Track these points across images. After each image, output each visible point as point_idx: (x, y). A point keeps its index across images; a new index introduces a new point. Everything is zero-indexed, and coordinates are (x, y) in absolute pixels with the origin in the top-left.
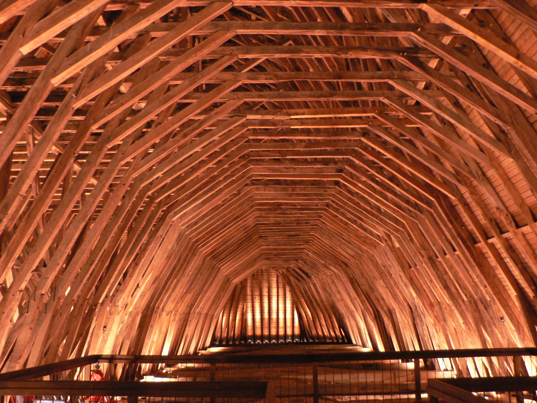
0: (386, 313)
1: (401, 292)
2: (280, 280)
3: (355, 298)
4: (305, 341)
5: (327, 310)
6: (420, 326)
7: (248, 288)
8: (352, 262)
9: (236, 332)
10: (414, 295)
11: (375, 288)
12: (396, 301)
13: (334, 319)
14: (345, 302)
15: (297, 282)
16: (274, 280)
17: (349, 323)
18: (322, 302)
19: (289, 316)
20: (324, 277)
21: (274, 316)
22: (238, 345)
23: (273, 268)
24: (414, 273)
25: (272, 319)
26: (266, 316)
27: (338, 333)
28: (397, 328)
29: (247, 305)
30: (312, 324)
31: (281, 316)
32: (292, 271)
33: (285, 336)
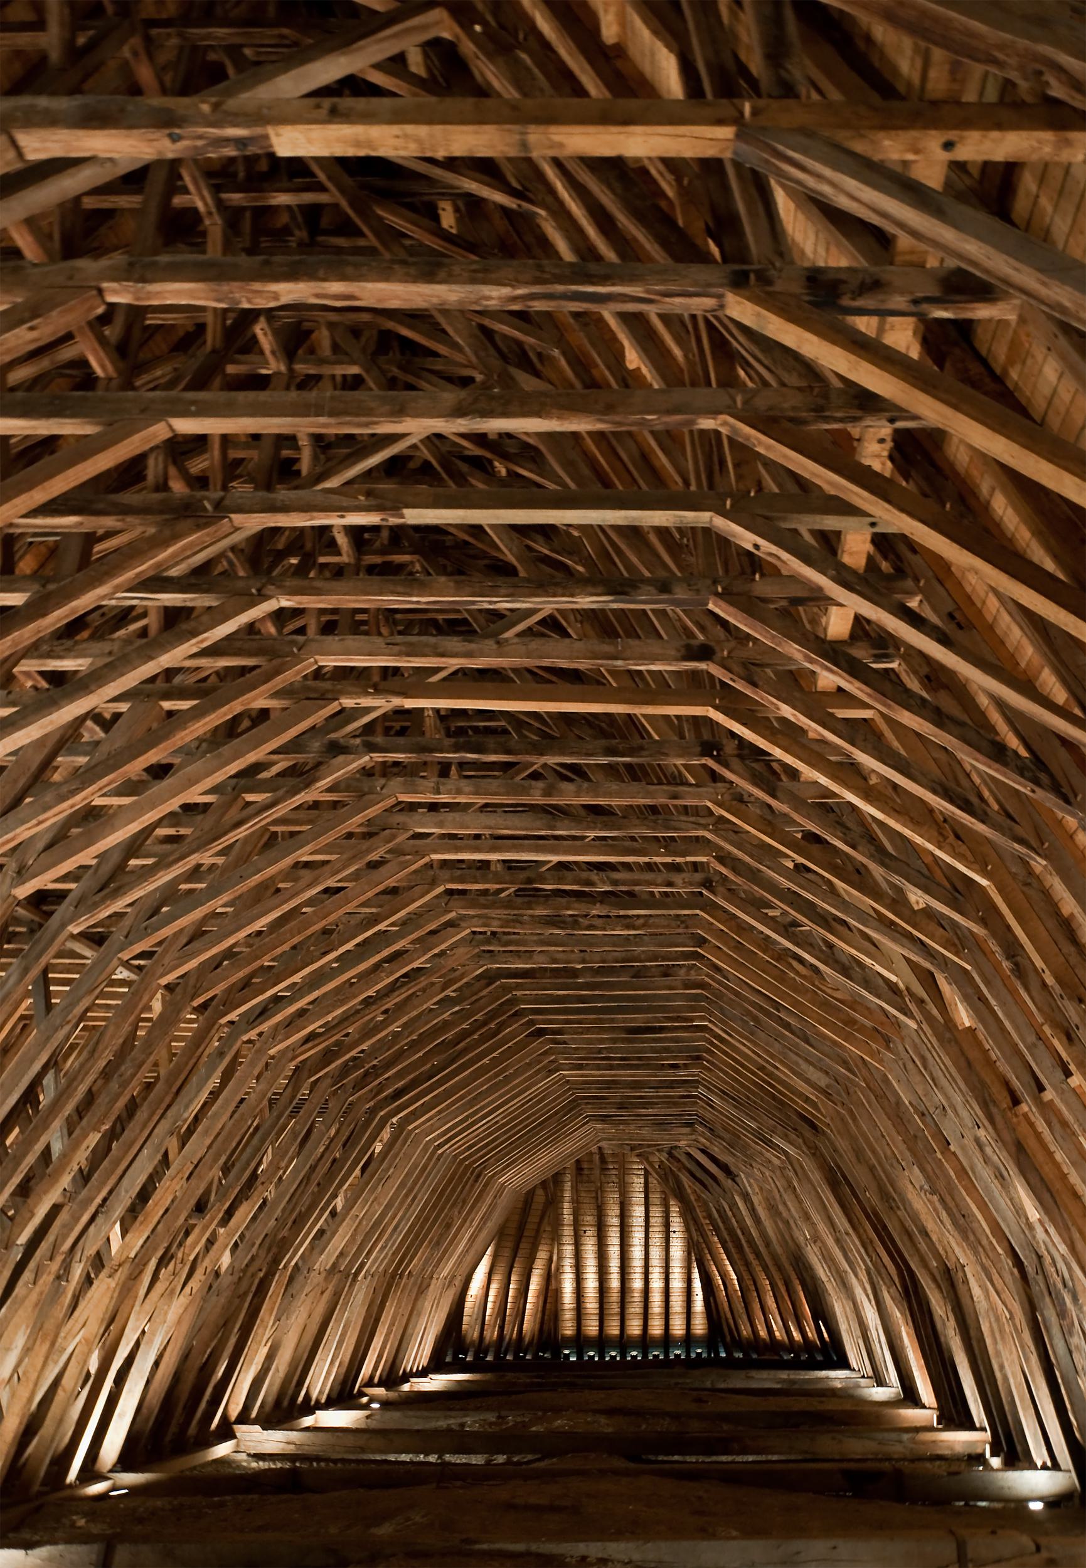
0: (934, 1280)
1: (983, 1207)
2: (653, 1181)
3: (847, 1234)
4: (723, 1355)
5: (780, 1268)
6: (1056, 1330)
7: (566, 1205)
8: (825, 1113)
9: (526, 1326)
10: (1034, 1214)
11: (899, 1194)
12: (966, 1238)
13: (801, 1294)
14: (824, 1243)
15: (698, 1187)
16: (637, 1184)
17: (840, 1309)
18: (768, 1244)
19: (677, 1284)
20: (767, 1173)
21: (637, 1284)
22: (510, 1367)
23: (633, 1148)
24: (1032, 1125)
25: (632, 1290)
26: (615, 1283)
27: (811, 1334)
28: (973, 1333)
29: (560, 1251)
30: (739, 1307)
31: (657, 1283)
32: (683, 1159)
33: (667, 1340)
